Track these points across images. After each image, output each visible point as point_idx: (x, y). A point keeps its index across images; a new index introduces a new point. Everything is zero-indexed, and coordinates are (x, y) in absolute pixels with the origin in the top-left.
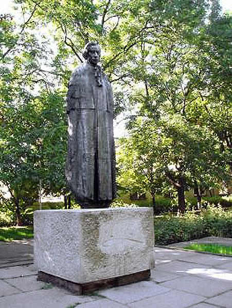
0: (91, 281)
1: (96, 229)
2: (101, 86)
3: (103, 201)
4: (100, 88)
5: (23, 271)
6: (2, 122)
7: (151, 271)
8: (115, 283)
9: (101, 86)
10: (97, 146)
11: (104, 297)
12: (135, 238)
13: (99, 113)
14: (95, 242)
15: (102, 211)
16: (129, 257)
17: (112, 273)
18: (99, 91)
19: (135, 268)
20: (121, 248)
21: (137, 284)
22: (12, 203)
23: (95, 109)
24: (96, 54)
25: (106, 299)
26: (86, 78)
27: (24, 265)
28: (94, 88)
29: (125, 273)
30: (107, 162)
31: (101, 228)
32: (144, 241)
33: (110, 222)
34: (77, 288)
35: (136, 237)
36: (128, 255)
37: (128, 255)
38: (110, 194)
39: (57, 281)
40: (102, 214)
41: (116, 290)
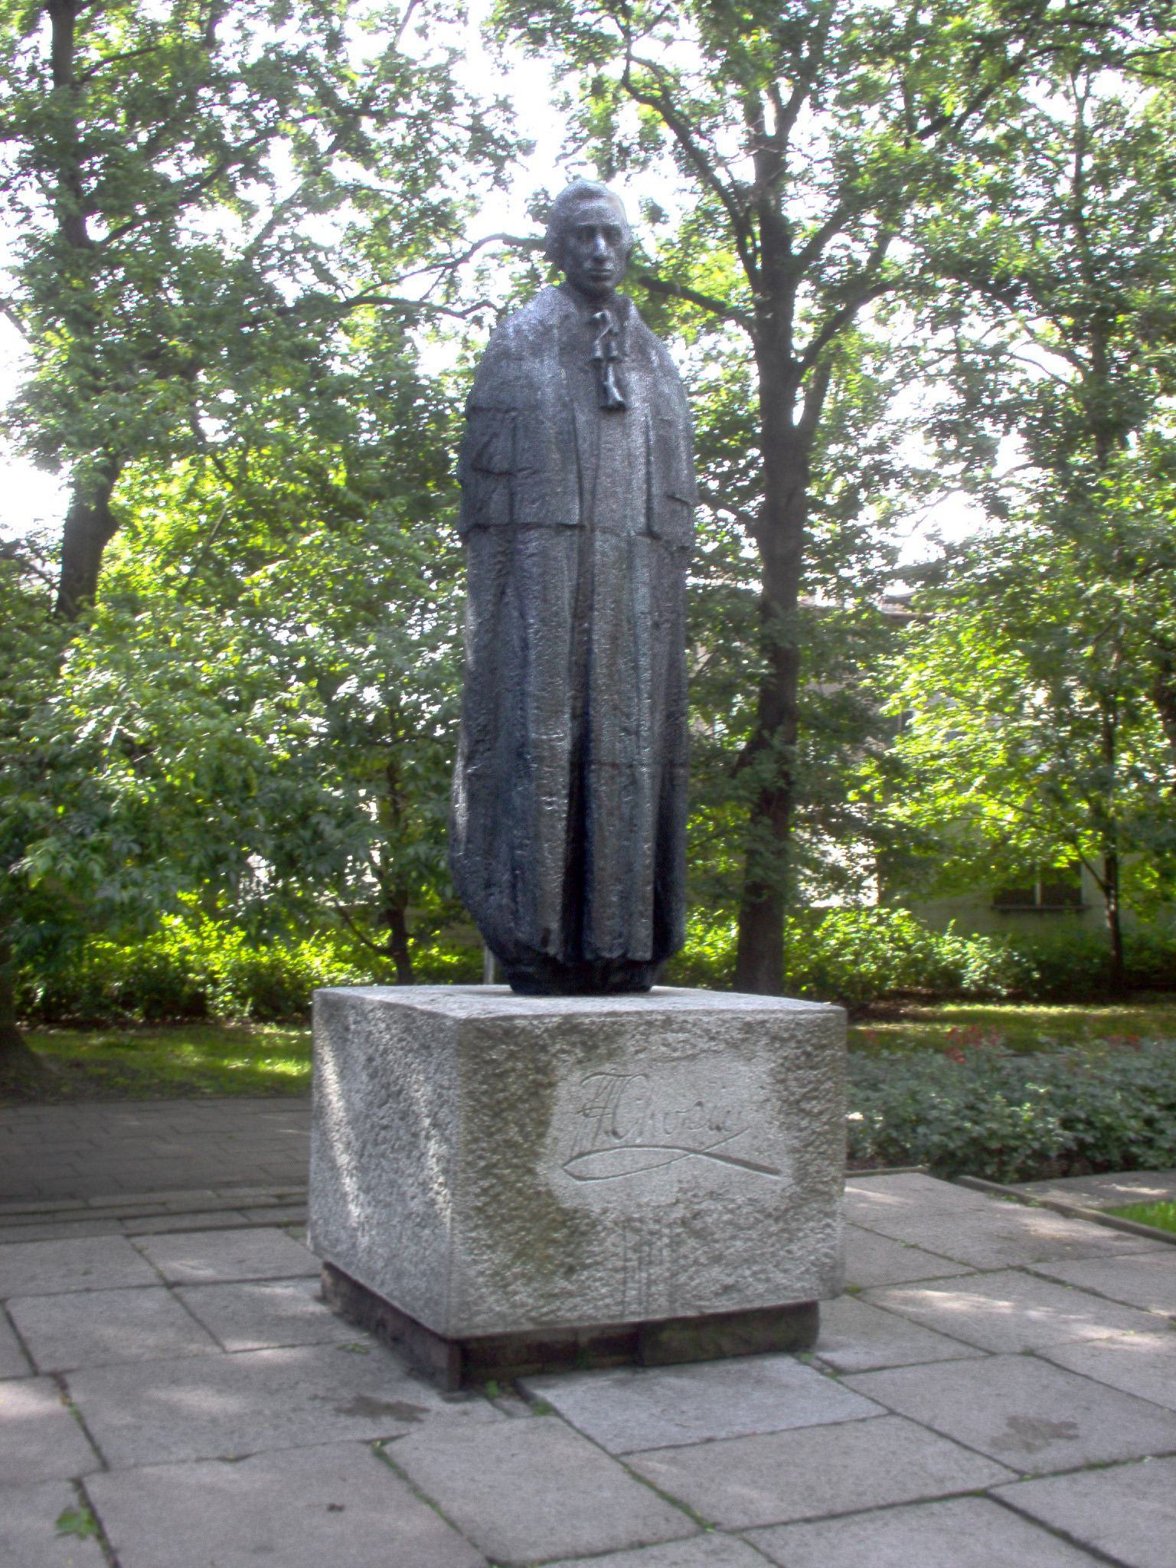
0: (499, 1330)
1: (536, 1094)
2: (621, 408)
3: (608, 966)
4: (615, 420)
5: (264, 1246)
6: (1172, 29)
7: (824, 1308)
8: (632, 1348)
9: (621, 408)
10: (586, 703)
11: (547, 1409)
12: (738, 1146)
13: (603, 545)
14: (525, 1154)
15: (567, 1018)
16: (699, 1234)
17: (600, 1299)
18: (611, 432)
19: (727, 1289)
20: (659, 1189)
21: (734, 1367)
22: (701, 813)
23: (580, 527)
24: (602, 243)
25: (553, 1420)
26: (548, 372)
27: (106, 1218)
28: (582, 418)
29: (647, 1312)
30: (634, 782)
31: (562, 1091)
32: (785, 1163)
33: (607, 1067)
34: (440, 1357)
35: (744, 1140)
36: (692, 1225)
37: (692, 1225)
38: (644, 930)
39: (380, 1312)
40: (569, 1027)
41: (623, 1383)
